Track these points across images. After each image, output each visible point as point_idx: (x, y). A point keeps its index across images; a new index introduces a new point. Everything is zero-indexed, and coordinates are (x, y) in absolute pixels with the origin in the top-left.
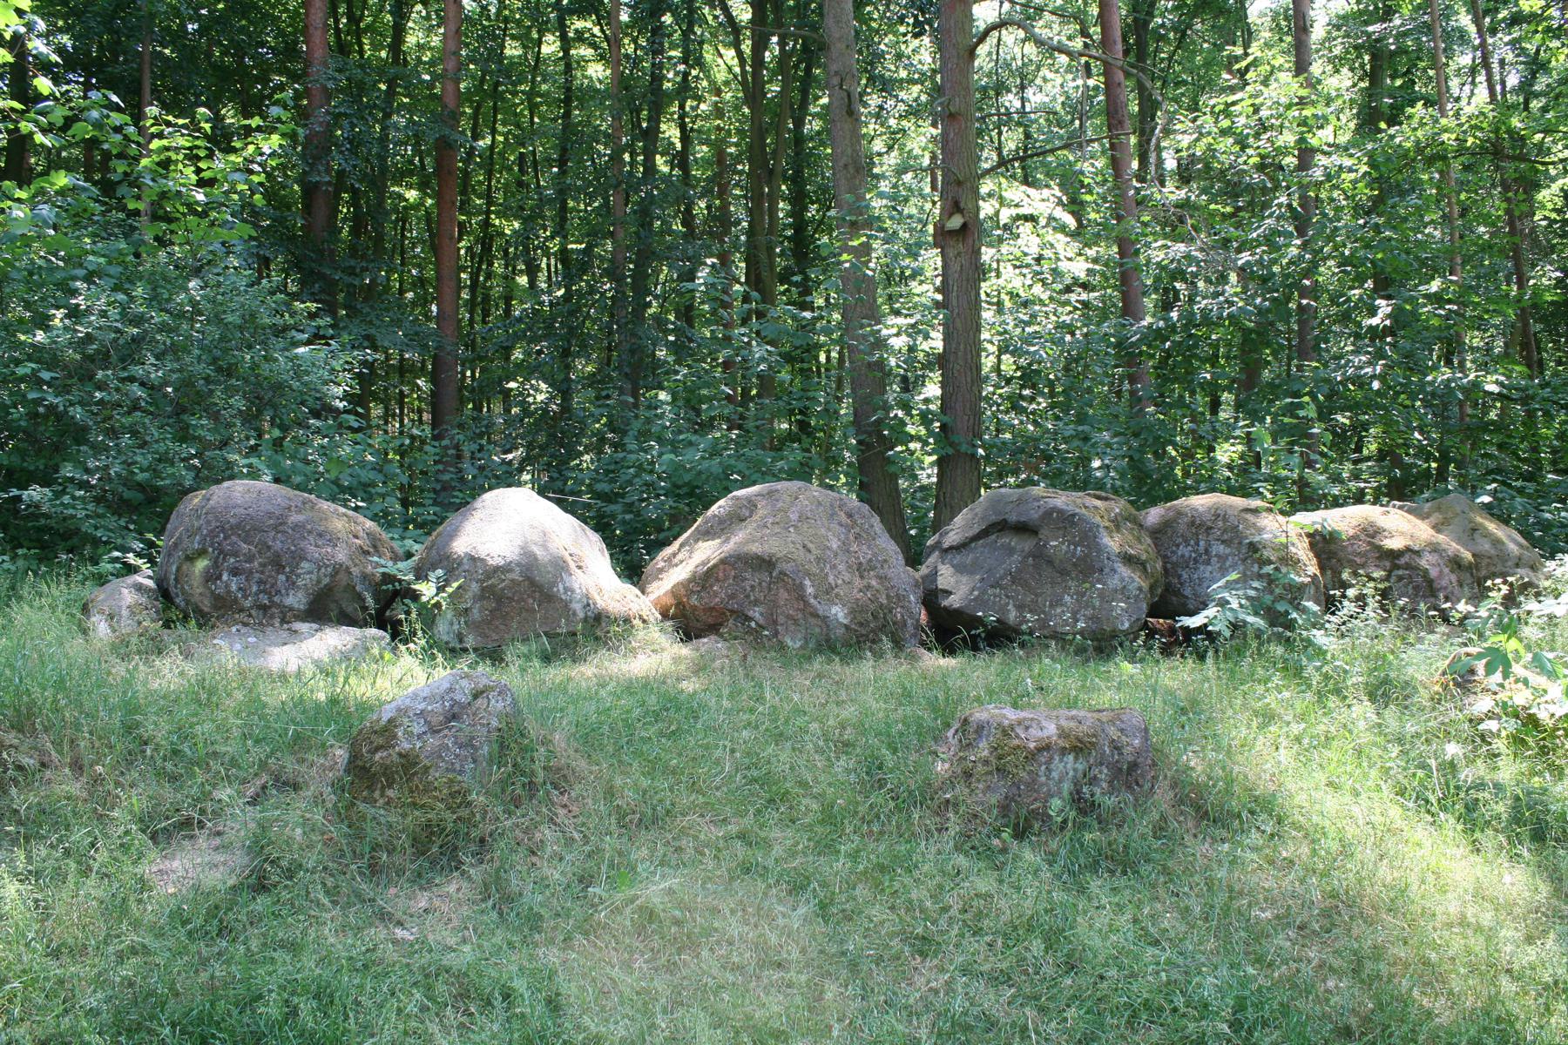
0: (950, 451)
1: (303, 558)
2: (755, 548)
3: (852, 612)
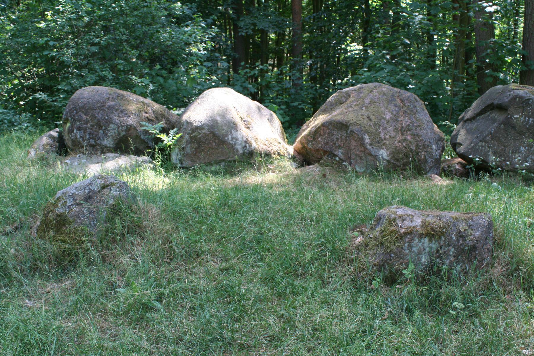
0: (525, 69)
1: (111, 122)
2: (339, 118)
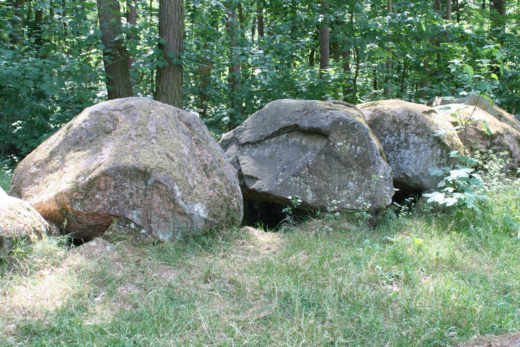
2: (129, 161)
3: (209, 207)
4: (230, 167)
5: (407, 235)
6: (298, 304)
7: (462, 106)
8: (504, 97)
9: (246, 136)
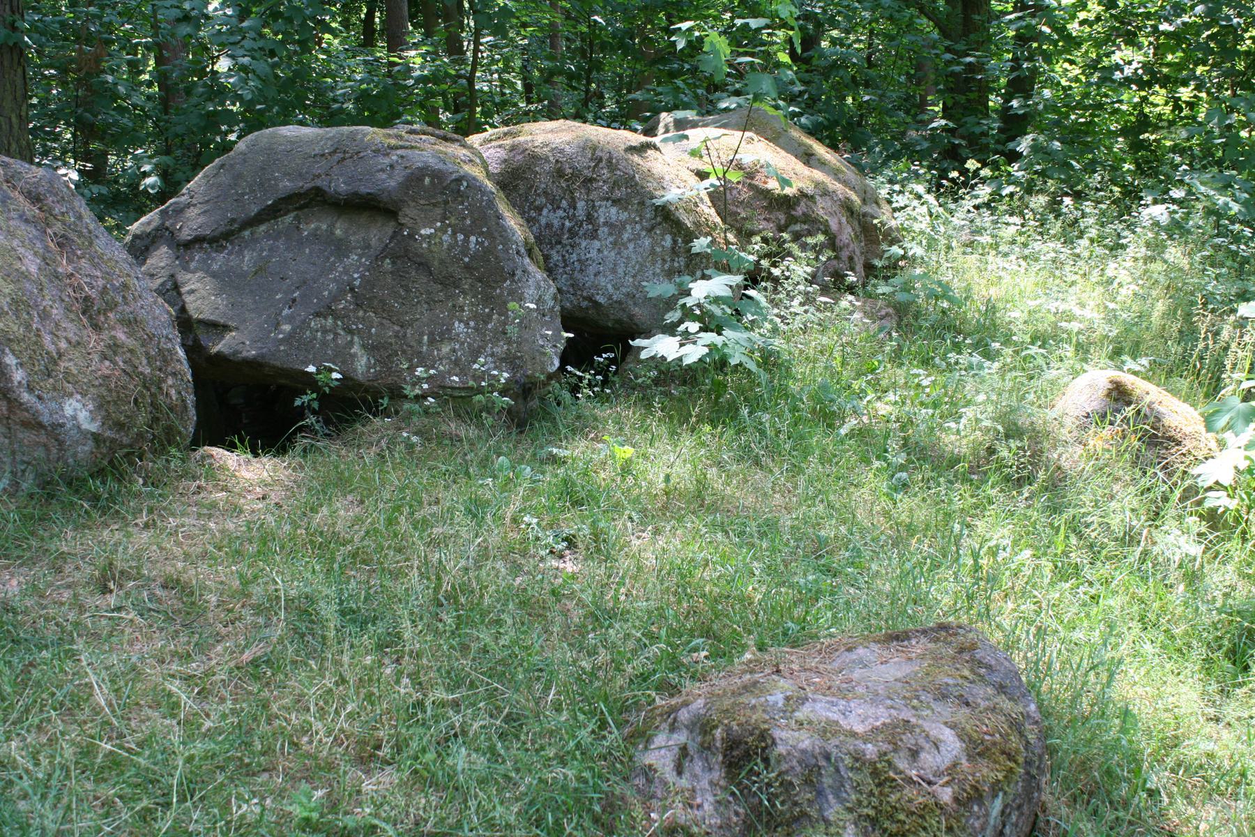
4: (155, 302)
5: (596, 439)
6: (333, 621)
7: (712, 132)
8: (820, 111)
9: (193, 223)
